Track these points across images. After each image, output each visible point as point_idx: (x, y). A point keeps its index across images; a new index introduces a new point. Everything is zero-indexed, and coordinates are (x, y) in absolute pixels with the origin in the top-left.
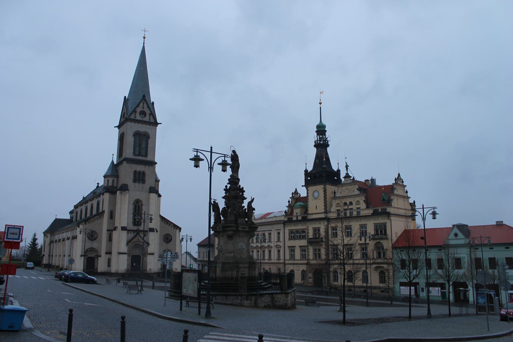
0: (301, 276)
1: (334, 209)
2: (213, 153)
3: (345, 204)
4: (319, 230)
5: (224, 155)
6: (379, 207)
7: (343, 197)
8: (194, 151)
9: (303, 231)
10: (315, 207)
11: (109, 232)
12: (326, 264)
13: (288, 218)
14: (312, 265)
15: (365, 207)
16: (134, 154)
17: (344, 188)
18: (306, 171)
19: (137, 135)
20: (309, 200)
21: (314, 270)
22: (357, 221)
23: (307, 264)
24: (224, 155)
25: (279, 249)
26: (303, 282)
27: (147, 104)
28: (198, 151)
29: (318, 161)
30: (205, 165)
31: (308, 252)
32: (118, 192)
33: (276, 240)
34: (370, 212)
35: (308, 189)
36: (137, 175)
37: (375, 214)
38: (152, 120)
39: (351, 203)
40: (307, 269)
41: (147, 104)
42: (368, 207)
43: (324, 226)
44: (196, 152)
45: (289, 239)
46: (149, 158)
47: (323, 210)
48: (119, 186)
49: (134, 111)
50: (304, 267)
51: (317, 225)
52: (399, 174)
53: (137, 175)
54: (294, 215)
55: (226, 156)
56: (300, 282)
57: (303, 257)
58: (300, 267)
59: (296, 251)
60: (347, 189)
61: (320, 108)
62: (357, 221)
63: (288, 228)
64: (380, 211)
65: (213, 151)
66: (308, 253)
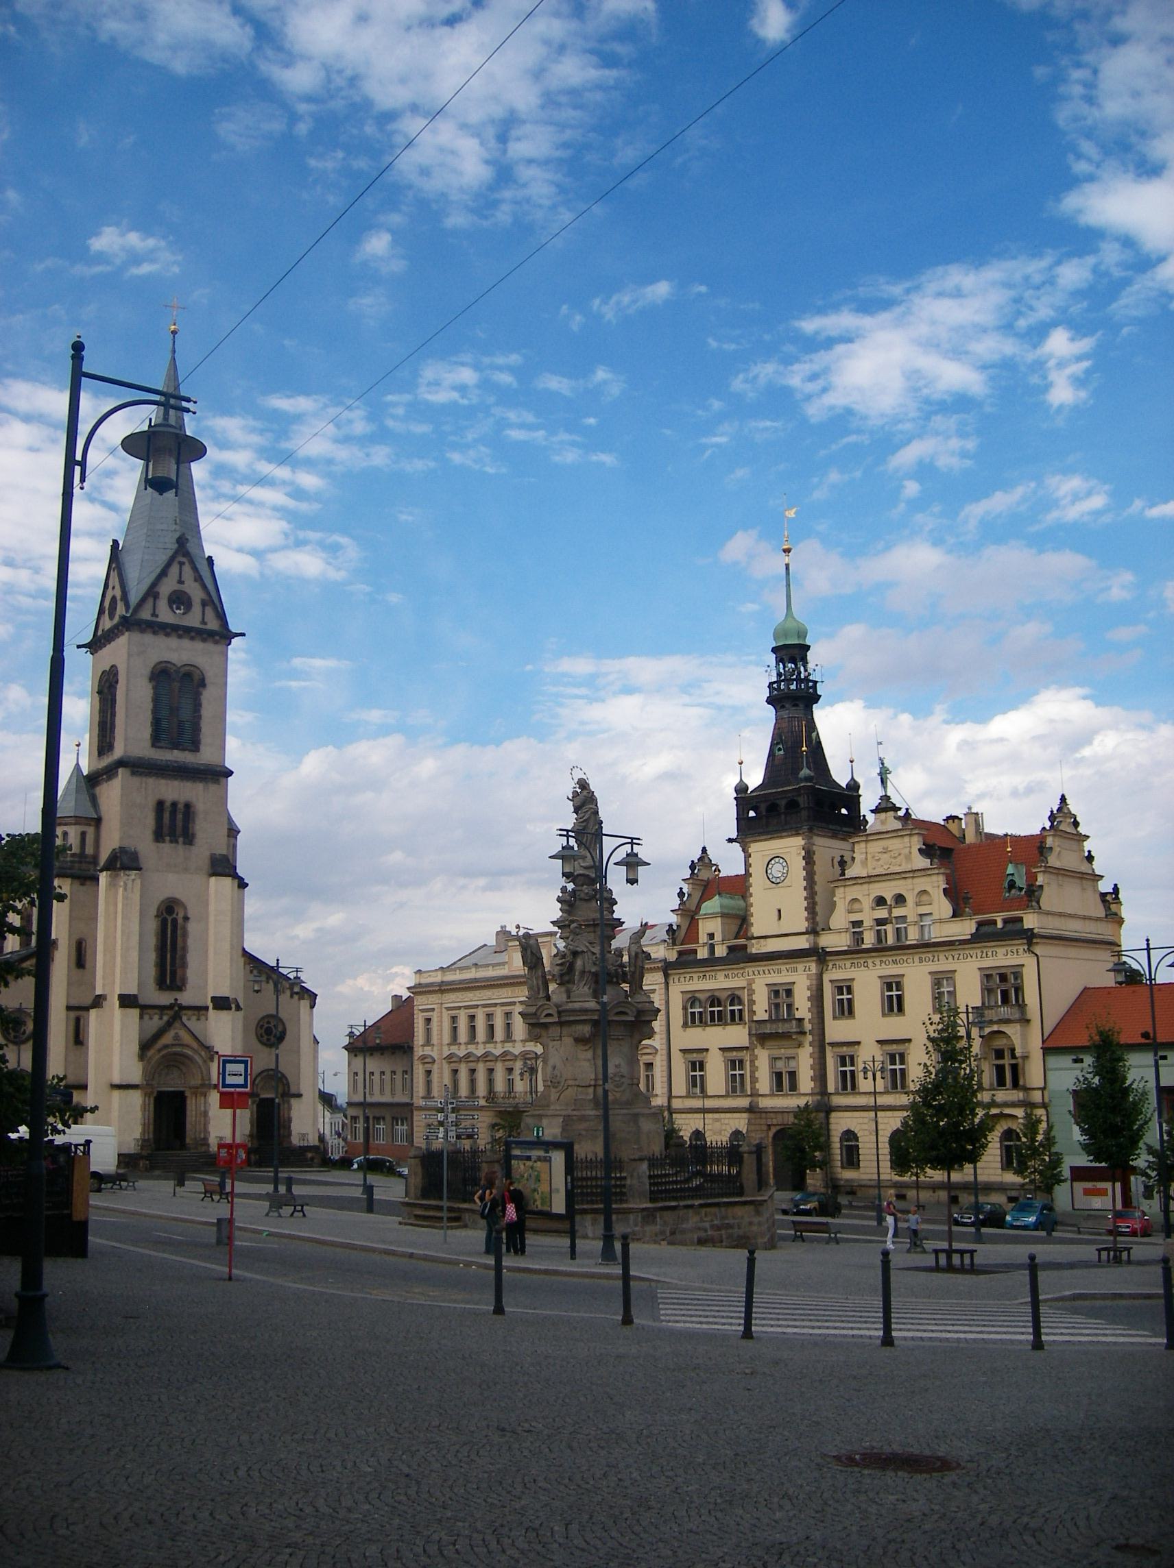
1: (840, 919)
3: (880, 901)
4: (789, 993)
5: (629, 840)
7: (871, 879)
9: (735, 999)
10: (777, 913)
11: (73, 1014)
14: (765, 1112)
15: (951, 913)
16: (156, 740)
17: (875, 847)
18: (741, 789)
19: (161, 675)
21: (774, 1130)
22: (921, 960)
23: (751, 1109)
24: (629, 840)
25: (428, 1067)
27: (195, 569)
31: (754, 1069)
32: (103, 878)
33: (447, 1038)
34: (966, 928)
36: (167, 816)
37: (985, 936)
38: (213, 625)
39: (900, 899)
41: (195, 569)
45: (685, 1025)
46: (205, 756)
47: (803, 926)
48: (104, 857)
49: (152, 593)
51: (781, 975)
53: (167, 816)
54: (701, 941)
55: (635, 841)
57: (736, 1084)
58: (726, 1121)
59: (708, 1067)
61: (787, 567)
62: (921, 960)
64: (1000, 925)
66: (752, 1073)
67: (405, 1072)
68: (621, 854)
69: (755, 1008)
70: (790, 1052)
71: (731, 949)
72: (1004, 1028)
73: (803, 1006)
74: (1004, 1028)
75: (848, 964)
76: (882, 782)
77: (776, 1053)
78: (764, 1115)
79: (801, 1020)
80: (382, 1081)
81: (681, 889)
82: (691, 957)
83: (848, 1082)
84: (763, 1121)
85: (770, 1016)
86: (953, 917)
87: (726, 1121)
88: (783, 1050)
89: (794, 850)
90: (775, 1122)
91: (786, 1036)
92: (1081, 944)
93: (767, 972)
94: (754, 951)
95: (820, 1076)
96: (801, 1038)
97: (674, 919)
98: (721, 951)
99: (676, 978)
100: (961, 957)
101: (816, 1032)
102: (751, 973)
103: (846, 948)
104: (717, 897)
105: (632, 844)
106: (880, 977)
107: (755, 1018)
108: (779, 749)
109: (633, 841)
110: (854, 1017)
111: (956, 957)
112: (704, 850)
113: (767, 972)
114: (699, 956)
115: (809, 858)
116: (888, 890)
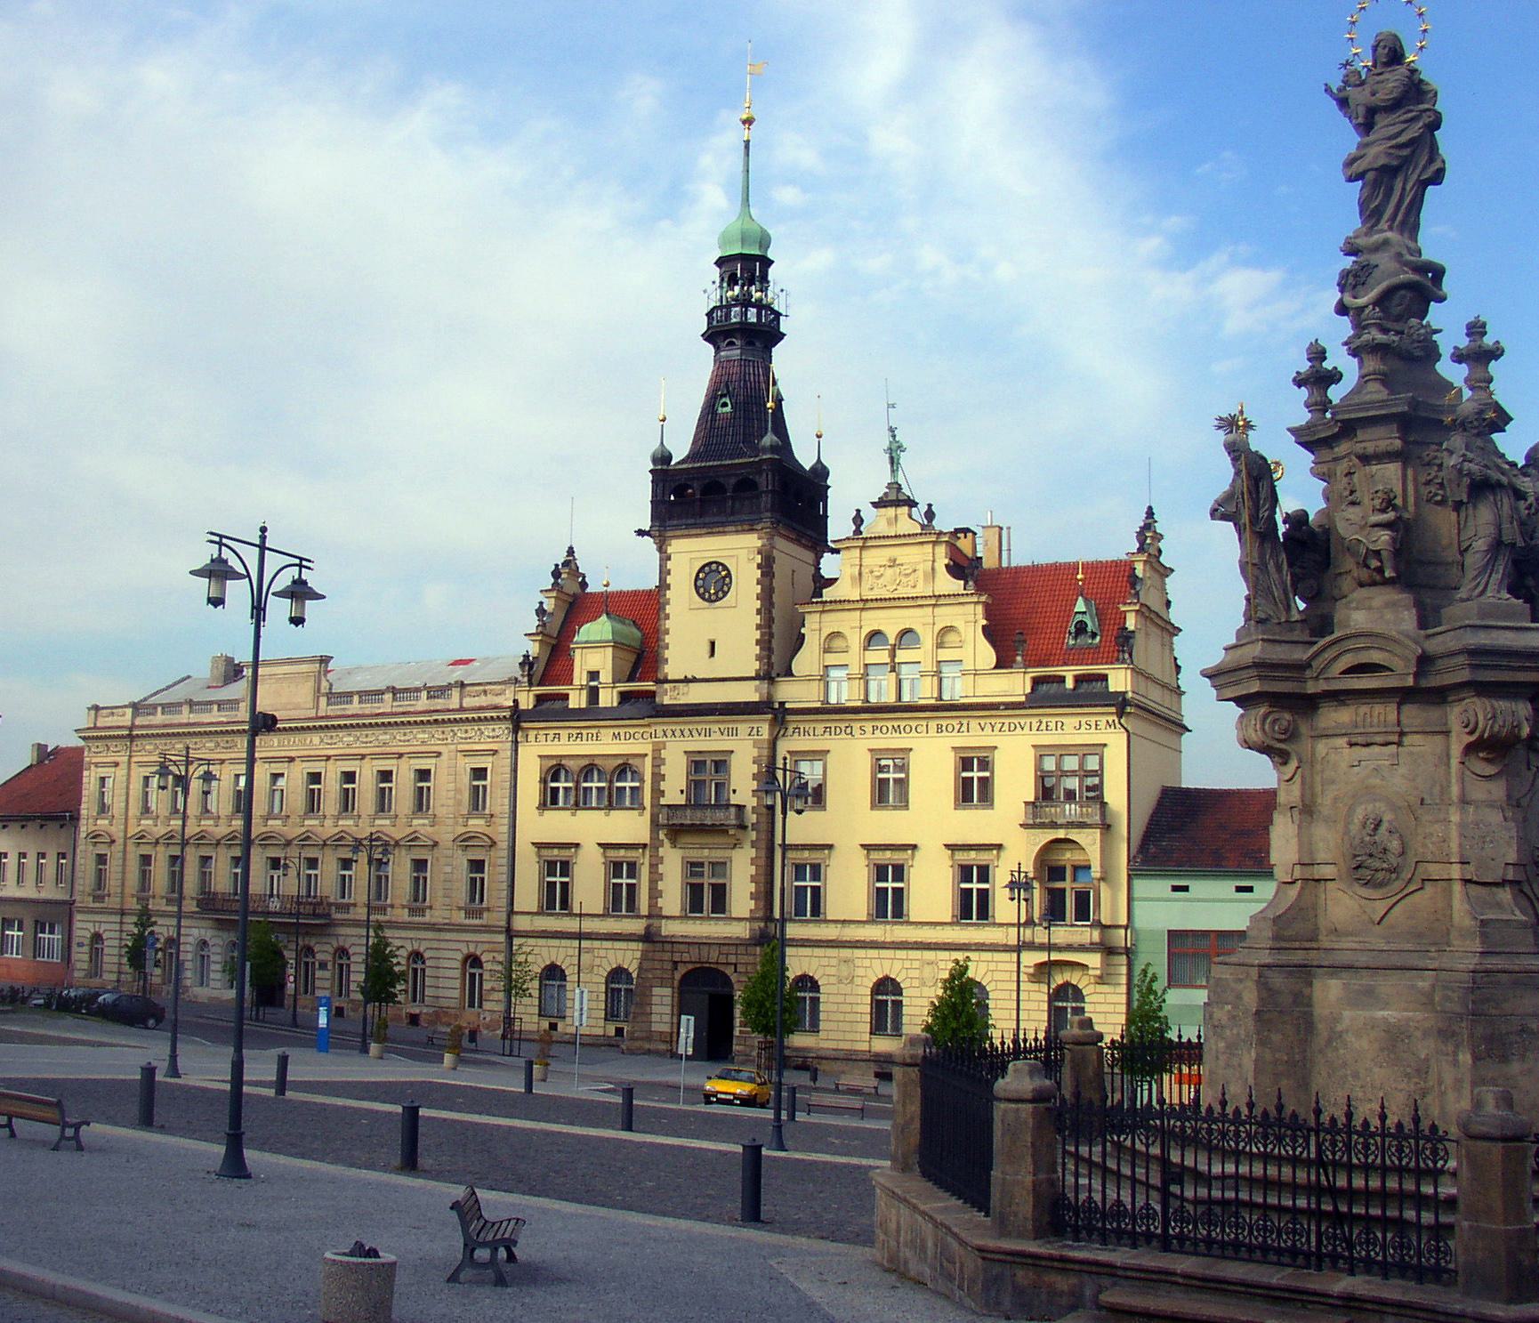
0: (603, 997)
2: (267, 552)
5: (297, 561)
6: (1065, 664)
7: (865, 604)
8: (309, 561)
9: (625, 768)
10: (707, 648)
12: (761, 939)
13: (540, 699)
14: (671, 942)
18: (662, 458)
20: (668, 609)
21: (682, 970)
22: (939, 729)
23: (648, 937)
24: (297, 561)
25: (102, 850)
26: (611, 1031)
28: (224, 541)
29: (728, 409)
30: (238, 593)
31: (655, 877)
35: (670, 550)
37: (1045, 696)
40: (646, 965)
42: (1003, 663)
43: (756, 744)
44: (217, 546)
45: (543, 806)
47: (752, 667)
50: (629, 957)
51: (710, 739)
52: (1150, 508)
54: (576, 682)
55: (304, 563)
56: (600, 1032)
57: (620, 899)
58: (602, 953)
60: (893, 563)
61: (747, 143)
62: (939, 729)
63: (537, 749)
64: (1070, 684)
65: (267, 545)
67: (63, 856)
68: (284, 581)
69: (663, 786)
70: (717, 855)
71: (625, 697)
72: (1074, 835)
73: (743, 786)
74: (1074, 835)
75: (820, 728)
76: (892, 463)
77: (695, 855)
78: (668, 947)
79: (740, 808)
80: (40, 867)
81: (541, 603)
82: (558, 705)
83: (812, 904)
84: (667, 956)
85: (688, 799)
86: (995, 668)
87: (602, 953)
88: (706, 852)
89: (743, 554)
90: (686, 957)
91: (718, 830)
92: (1162, 722)
93: (687, 733)
94: (667, 701)
95: (765, 895)
96: (740, 834)
97: (533, 649)
98: (608, 698)
99: (532, 734)
100: (1006, 728)
101: (764, 827)
102: (660, 733)
103: (818, 705)
104: (604, 617)
105: (209, 764)
106: (871, 750)
107: (663, 801)
108: (725, 405)
109: (302, 563)
110: (991, 806)
111: (1035, 726)
112: (571, 551)
113: (687, 733)
114: (573, 704)
115: (767, 567)
116: (890, 623)
